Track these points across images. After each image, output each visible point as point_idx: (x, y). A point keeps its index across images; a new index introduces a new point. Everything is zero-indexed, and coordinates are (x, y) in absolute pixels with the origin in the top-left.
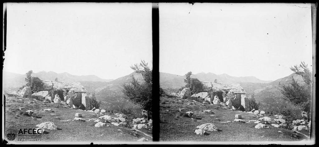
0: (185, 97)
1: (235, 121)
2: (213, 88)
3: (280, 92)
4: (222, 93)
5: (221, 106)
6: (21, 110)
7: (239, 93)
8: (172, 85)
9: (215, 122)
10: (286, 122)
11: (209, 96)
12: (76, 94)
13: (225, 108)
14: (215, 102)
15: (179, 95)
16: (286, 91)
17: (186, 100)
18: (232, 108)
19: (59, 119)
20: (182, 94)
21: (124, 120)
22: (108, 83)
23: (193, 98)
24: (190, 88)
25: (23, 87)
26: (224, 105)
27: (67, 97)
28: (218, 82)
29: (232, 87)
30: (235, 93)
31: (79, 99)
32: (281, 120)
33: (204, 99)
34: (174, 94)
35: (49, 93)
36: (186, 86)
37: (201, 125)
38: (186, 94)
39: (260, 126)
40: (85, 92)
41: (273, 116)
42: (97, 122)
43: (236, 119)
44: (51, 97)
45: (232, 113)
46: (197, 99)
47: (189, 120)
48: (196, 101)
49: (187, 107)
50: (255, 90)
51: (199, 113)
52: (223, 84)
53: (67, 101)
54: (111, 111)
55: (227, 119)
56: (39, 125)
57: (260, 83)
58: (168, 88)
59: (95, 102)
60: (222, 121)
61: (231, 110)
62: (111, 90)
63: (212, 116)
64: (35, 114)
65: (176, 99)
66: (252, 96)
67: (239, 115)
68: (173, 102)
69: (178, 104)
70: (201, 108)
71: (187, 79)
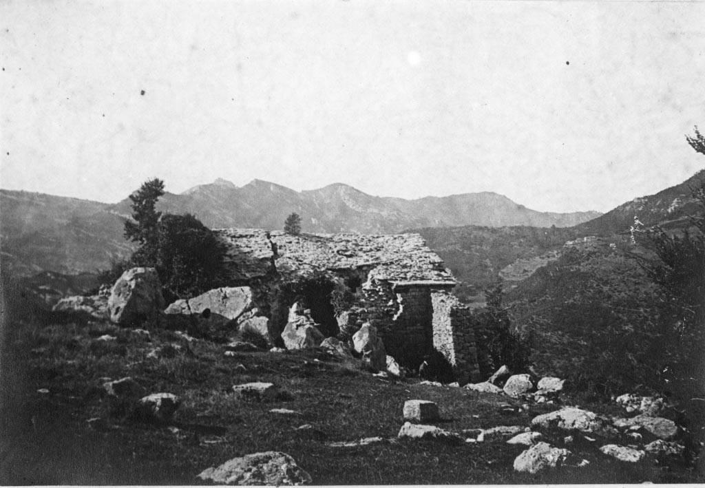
0: (132, 317)
1: (406, 437)
2: (278, 263)
3: (641, 271)
4: (332, 286)
5: (325, 356)
6: (111, 392)
7: (418, 282)
8: (64, 257)
9: (297, 447)
10: (680, 431)
11: (261, 303)
12: (399, 300)
13: (350, 366)
14: (292, 336)
15: (103, 309)
16: (668, 262)
17: (138, 331)
18: (384, 367)
19: (321, 436)
20: (115, 301)
21: (667, 426)
22: (571, 233)
23: (180, 321)
24: (157, 268)
25: (119, 270)
26: (340, 350)
27: (353, 318)
28: (302, 232)
29: (379, 254)
30: (395, 283)
31: (419, 326)
32: (648, 422)
33: (233, 324)
34: (74, 301)
35: (256, 301)
36: (137, 260)
37: (223, 461)
38: (139, 301)
39: (540, 458)
40: (447, 288)
41: (608, 401)
42: (522, 448)
43: (407, 424)
44: (269, 316)
45: (385, 394)
46: (196, 324)
47: (159, 437)
48: (190, 335)
49: (143, 369)
50: (505, 265)
51: (211, 400)
52: (331, 240)
53: (356, 335)
54: (591, 385)
55: (362, 427)
56: (217, 472)
57: (532, 229)
58: (39, 269)
59: (501, 339)
60: (336, 441)
61: (378, 379)
62: (584, 267)
63: (282, 411)
64: (190, 414)
65: (87, 330)
66: (492, 296)
67: (421, 405)
68: (72, 346)
69: (99, 357)
70: (219, 370)
71: (136, 218)
